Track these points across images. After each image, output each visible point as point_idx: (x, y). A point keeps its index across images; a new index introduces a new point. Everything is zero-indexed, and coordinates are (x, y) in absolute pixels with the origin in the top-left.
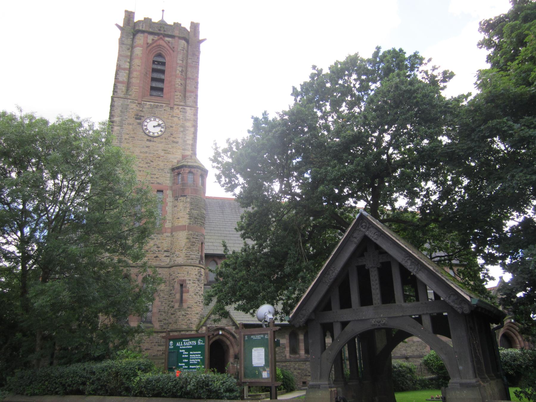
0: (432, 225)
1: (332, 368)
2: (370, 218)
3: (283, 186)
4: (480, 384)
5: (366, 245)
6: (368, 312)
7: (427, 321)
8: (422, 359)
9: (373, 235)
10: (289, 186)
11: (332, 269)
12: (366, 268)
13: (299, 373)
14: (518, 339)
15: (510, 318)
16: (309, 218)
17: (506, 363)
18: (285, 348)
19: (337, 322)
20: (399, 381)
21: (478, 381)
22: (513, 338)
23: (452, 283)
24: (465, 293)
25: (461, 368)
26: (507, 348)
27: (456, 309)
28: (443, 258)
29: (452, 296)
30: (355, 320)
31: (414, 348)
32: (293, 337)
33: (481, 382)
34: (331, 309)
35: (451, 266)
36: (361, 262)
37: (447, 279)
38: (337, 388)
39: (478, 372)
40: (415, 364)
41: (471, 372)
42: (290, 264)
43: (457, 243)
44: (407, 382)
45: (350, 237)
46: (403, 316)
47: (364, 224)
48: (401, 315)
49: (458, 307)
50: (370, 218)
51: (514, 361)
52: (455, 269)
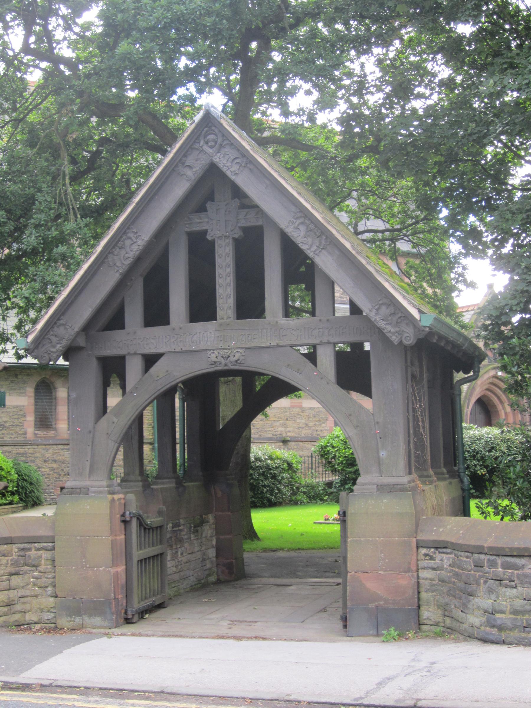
0: (363, 162)
1: (117, 450)
2: (227, 124)
3: (32, 39)
4: (417, 487)
5: (212, 187)
6: (204, 334)
7: (327, 360)
8: (316, 444)
9: (229, 164)
10: (47, 35)
11: (131, 235)
12: (209, 238)
13: (53, 469)
14: (504, 408)
15: (495, 368)
16: (88, 120)
17: (474, 455)
18: (24, 416)
19: (135, 354)
20: (264, 486)
21: (414, 481)
22: (494, 406)
23: (387, 280)
24: (410, 303)
25: (383, 454)
26: (482, 426)
27: (389, 335)
28: (380, 236)
29: (384, 308)
30: (175, 352)
31: (302, 422)
32: (45, 389)
33: (418, 482)
34: (123, 327)
35: (395, 255)
36: (199, 223)
37: (377, 271)
38: (126, 493)
39: (416, 464)
40: (302, 453)
41: (402, 463)
42: (37, 226)
43: (412, 207)
44: (279, 489)
45: (177, 166)
46: (278, 346)
47: (211, 137)
48: (274, 343)
49: (393, 330)
50: (227, 124)
51: (490, 451)
52: (402, 261)
